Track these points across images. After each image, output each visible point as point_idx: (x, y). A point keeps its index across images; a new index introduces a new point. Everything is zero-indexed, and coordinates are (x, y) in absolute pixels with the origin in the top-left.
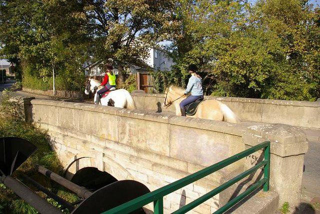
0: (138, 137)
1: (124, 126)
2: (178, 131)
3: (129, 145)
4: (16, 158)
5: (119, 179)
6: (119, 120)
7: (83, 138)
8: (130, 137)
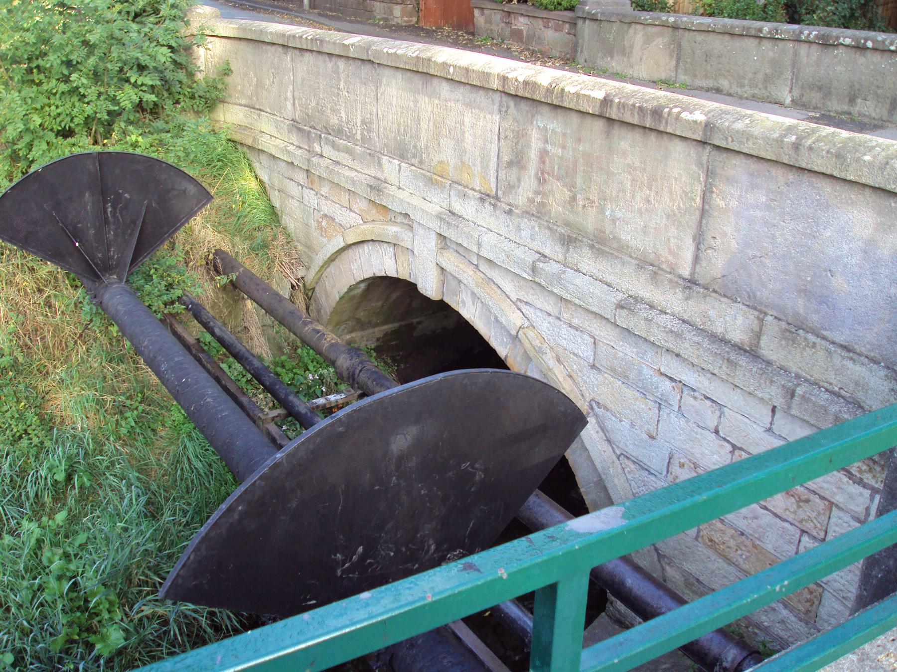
0: (572, 186)
1: (520, 137)
2: (744, 179)
3: (537, 212)
4: (827, 653)
5: (422, 291)
6: (503, 112)
7: (372, 172)
8: (541, 181)
